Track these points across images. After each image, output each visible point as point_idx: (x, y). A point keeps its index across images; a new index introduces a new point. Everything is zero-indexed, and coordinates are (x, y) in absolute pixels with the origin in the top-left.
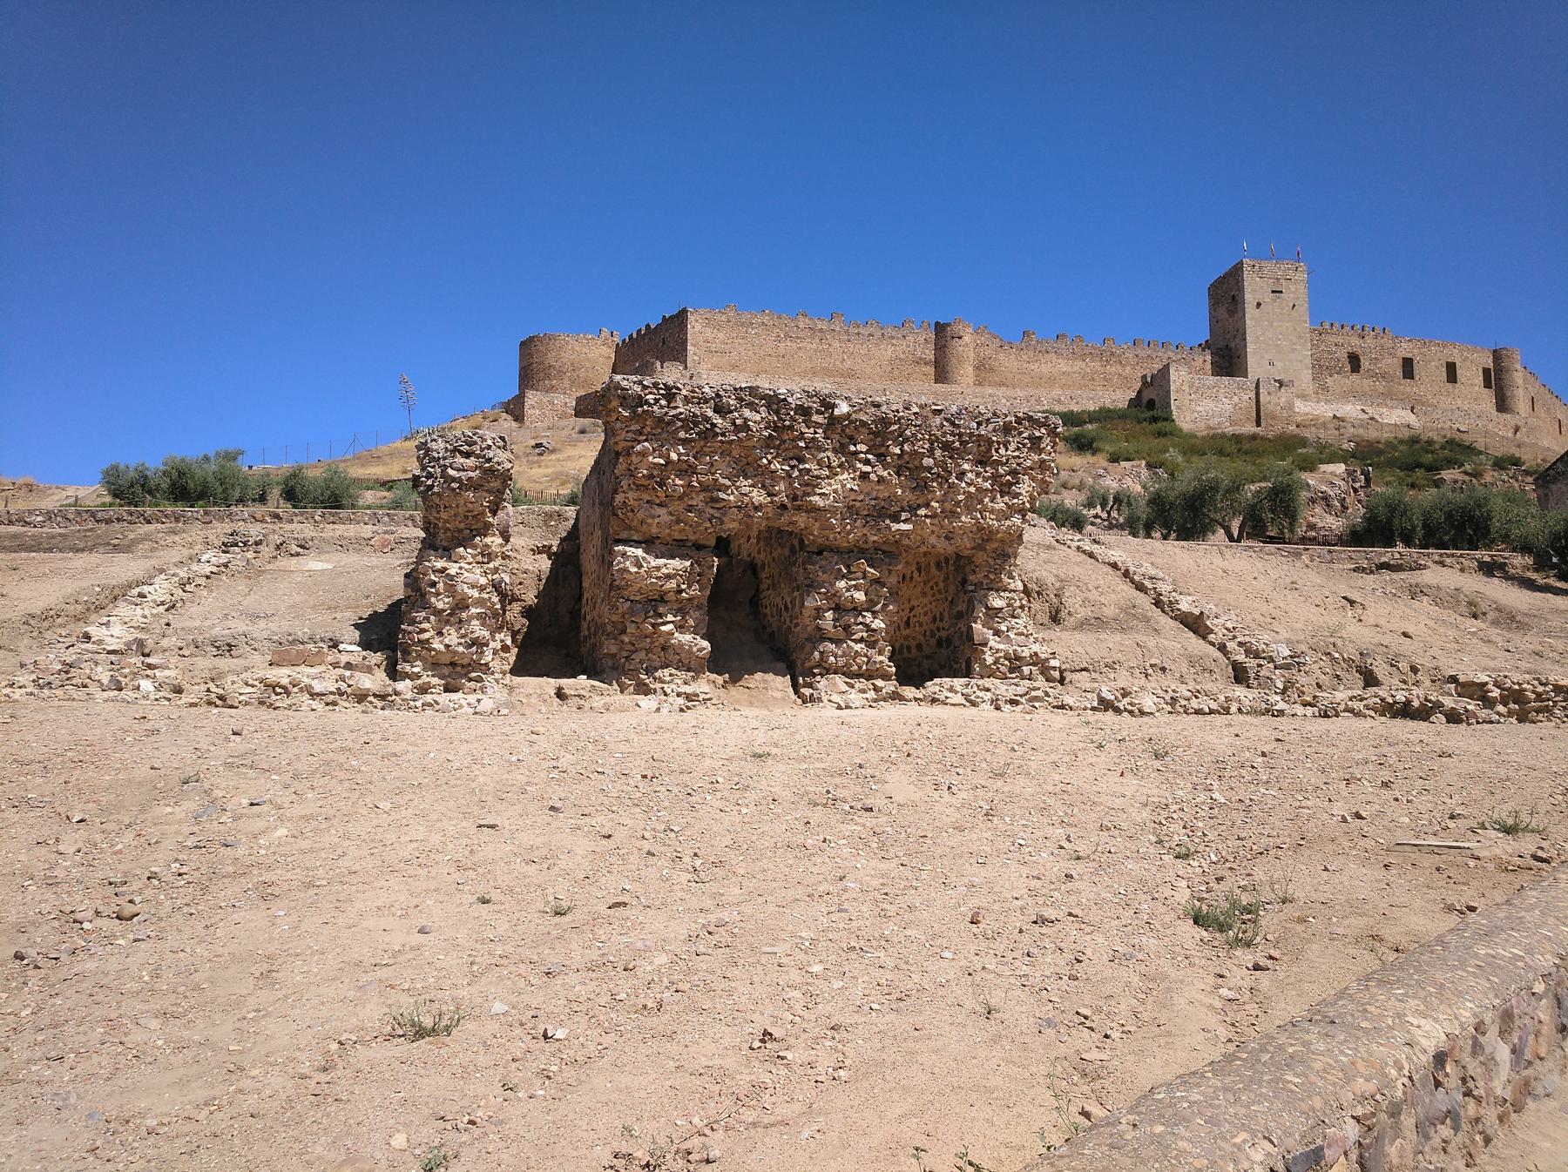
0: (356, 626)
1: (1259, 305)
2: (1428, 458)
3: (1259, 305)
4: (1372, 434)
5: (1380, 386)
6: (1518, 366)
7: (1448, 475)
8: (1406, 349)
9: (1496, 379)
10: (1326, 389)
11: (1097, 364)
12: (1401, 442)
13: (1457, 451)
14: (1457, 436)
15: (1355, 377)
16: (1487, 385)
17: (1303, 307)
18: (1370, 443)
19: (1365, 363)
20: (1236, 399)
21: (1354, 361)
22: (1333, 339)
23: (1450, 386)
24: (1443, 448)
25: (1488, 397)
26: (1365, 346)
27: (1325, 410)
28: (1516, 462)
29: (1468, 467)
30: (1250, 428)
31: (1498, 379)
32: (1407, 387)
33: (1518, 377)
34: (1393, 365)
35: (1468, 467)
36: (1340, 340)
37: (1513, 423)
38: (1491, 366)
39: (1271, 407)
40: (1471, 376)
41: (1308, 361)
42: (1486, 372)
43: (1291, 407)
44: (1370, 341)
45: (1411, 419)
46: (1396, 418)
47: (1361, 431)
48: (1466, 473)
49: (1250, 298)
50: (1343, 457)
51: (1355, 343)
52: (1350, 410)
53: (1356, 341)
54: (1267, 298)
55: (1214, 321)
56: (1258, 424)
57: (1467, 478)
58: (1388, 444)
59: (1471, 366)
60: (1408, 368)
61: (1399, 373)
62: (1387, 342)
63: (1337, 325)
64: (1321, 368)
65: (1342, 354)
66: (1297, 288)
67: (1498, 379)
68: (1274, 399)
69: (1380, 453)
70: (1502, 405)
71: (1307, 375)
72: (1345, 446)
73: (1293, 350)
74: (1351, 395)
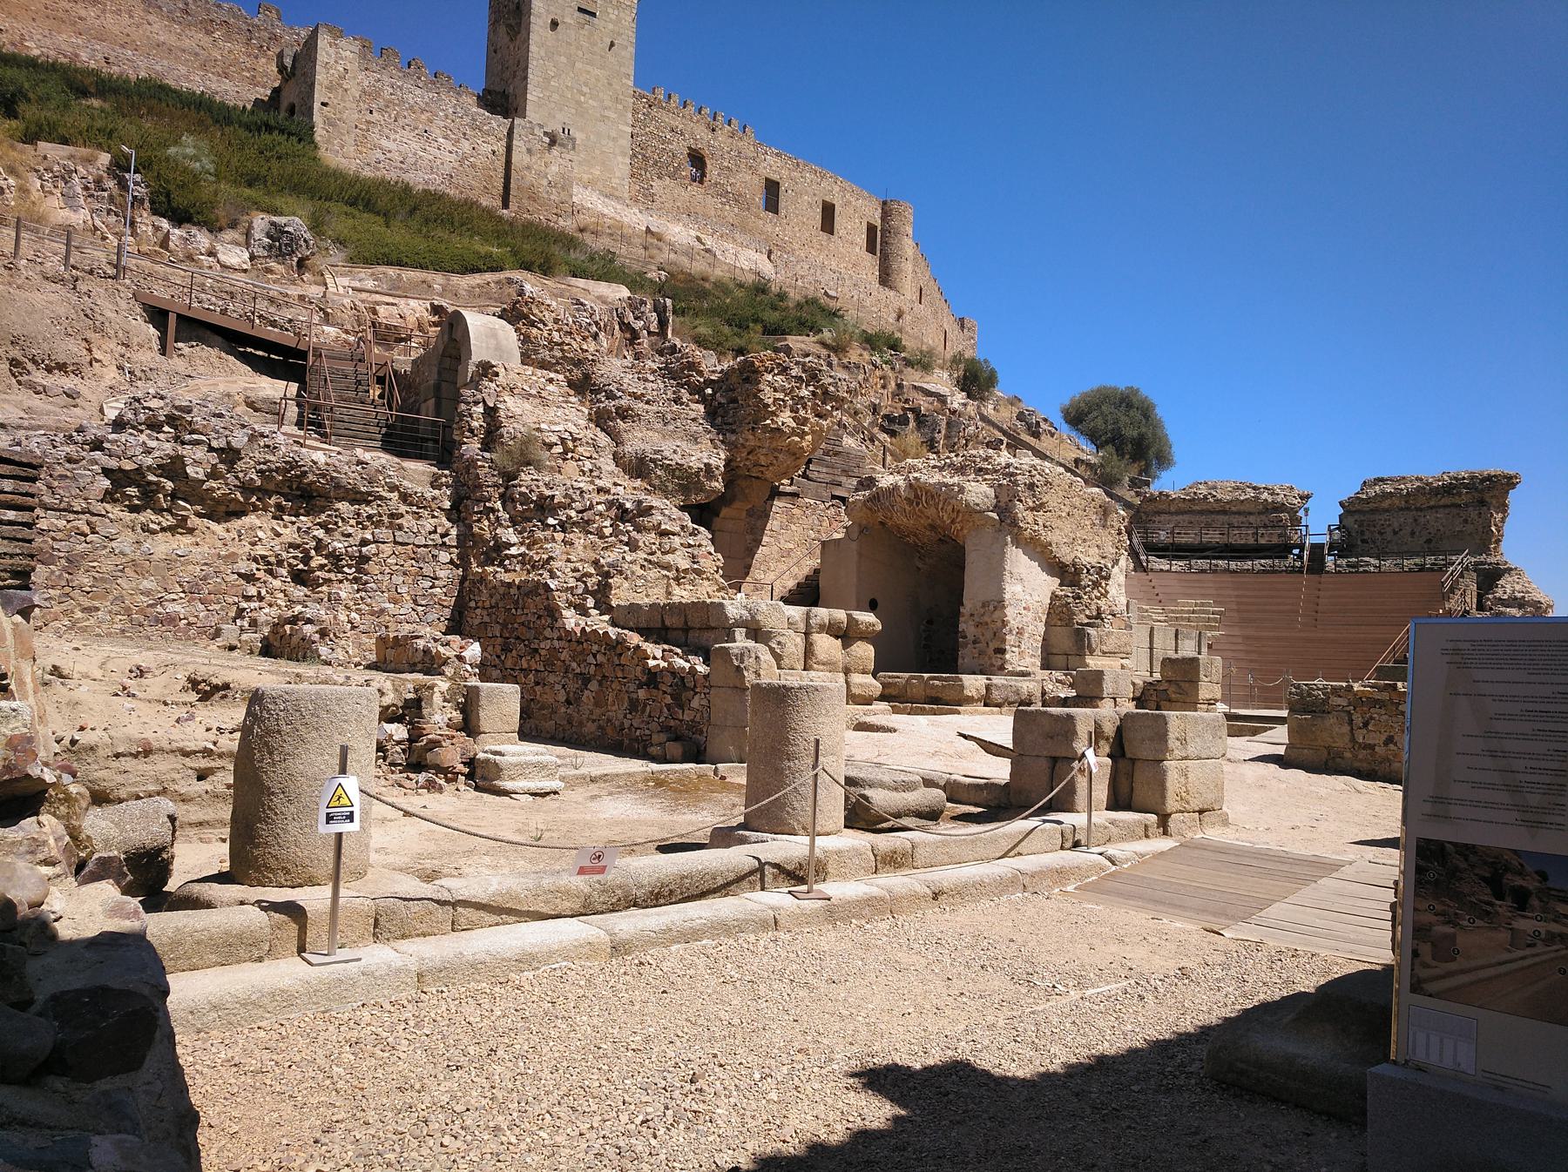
0: (1341, 504)
1: (554, 24)
2: (772, 317)
3: (554, 24)
4: (698, 267)
5: (731, 212)
6: (910, 231)
7: (795, 342)
8: (773, 165)
9: (879, 241)
10: (652, 198)
11: (237, 48)
12: (741, 286)
13: (814, 315)
14: (823, 301)
15: (694, 189)
16: (871, 248)
17: (627, 52)
18: (690, 278)
20: (466, 146)
21: (697, 159)
22: (668, 119)
23: (824, 236)
24: (799, 306)
25: (870, 265)
26: (719, 144)
27: (635, 218)
28: (895, 346)
29: (827, 335)
30: (490, 201)
31: (884, 243)
32: (767, 223)
33: (907, 247)
35: (827, 335)
36: (678, 123)
37: (896, 304)
38: (878, 223)
39: (530, 177)
40: (852, 228)
41: (626, 142)
42: (871, 229)
43: (565, 185)
44: (722, 140)
45: (767, 268)
46: (743, 259)
47: (685, 261)
48: (824, 344)
50: (635, 282)
51: (701, 136)
52: (680, 233)
53: (702, 133)
54: (570, 18)
55: (493, 49)
56: (506, 205)
57: (824, 352)
58: (719, 285)
59: (857, 213)
60: (772, 189)
61: (760, 199)
62: (747, 145)
63: (676, 98)
64: (645, 162)
65: (680, 148)
67: (884, 243)
68: (537, 163)
69: (703, 294)
70: (886, 278)
71: (622, 165)
72: (652, 275)
73: (604, 118)
74: (689, 213)
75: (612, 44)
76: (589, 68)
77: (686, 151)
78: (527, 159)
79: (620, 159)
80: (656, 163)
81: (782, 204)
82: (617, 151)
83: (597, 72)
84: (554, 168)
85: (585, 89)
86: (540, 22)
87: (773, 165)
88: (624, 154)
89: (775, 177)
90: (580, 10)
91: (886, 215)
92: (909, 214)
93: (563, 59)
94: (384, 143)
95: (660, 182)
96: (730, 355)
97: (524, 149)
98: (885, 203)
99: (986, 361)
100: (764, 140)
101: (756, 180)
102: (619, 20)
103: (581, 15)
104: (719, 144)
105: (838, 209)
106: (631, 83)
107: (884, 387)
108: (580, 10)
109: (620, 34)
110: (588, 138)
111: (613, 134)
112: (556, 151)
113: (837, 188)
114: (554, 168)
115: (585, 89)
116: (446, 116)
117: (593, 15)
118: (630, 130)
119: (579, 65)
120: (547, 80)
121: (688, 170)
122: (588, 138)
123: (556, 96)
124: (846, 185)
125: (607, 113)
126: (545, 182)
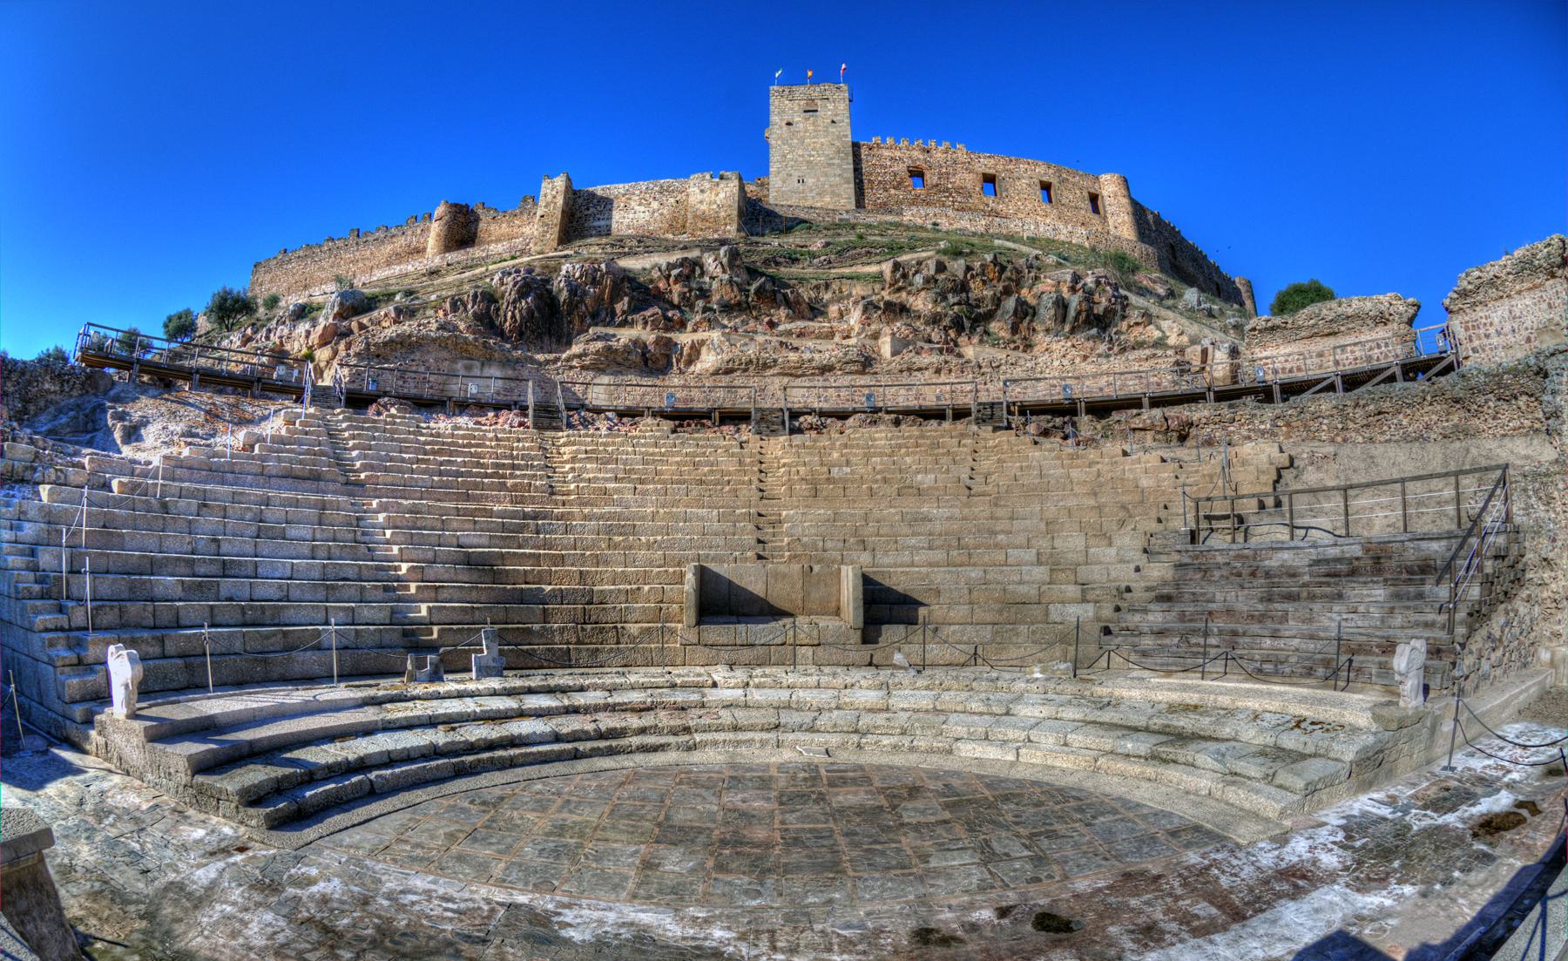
19: (931, 178)
34: (969, 180)
65: (900, 168)
66: (836, 104)
84: (722, 195)
87: (986, 163)
94: (596, 224)
114: (722, 195)
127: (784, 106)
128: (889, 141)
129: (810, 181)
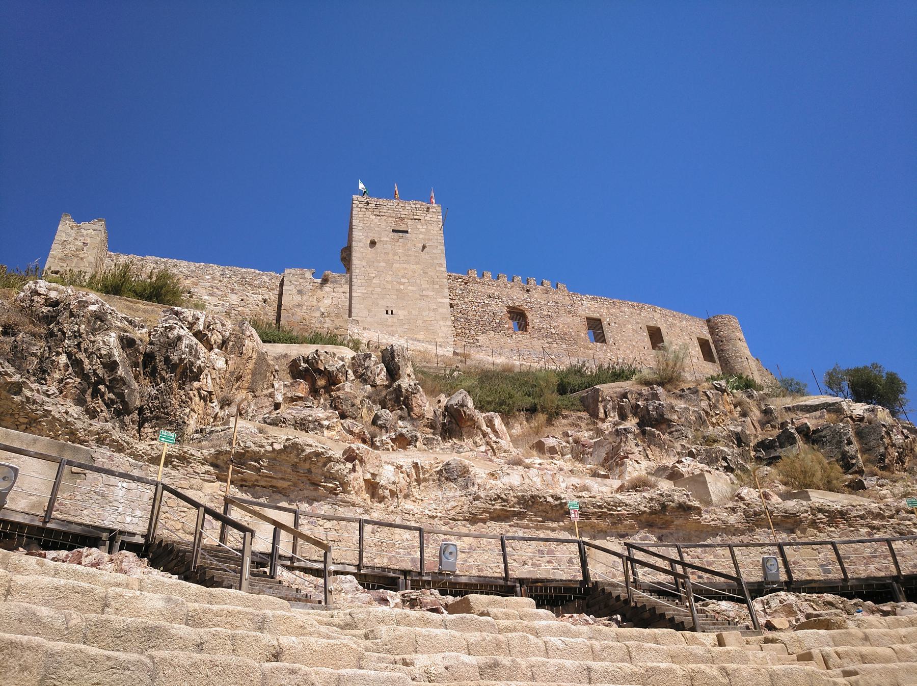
1: (373, 243)
3: (373, 243)
15: (520, 336)
19: (533, 319)
20: (234, 299)
38: (708, 337)
41: (446, 310)
42: (704, 344)
49: (360, 238)
51: (517, 296)
54: (387, 237)
61: (584, 333)
62: (562, 296)
65: (500, 308)
66: (428, 224)
68: (309, 300)
73: (423, 297)
75: (424, 247)
76: (405, 266)
77: (505, 310)
78: (298, 298)
79: (442, 323)
80: (478, 323)
81: (608, 334)
82: (438, 318)
83: (415, 267)
84: (327, 302)
85: (403, 280)
86: (361, 244)
87: (589, 306)
88: (445, 319)
89: (596, 315)
90: (394, 231)
91: (713, 329)
92: (735, 322)
93: (382, 264)
95: (485, 336)
96: (522, 417)
97: (295, 291)
98: (708, 321)
99: (875, 366)
100: (577, 288)
101: (577, 320)
102: (428, 231)
103: (396, 234)
104: (537, 299)
105: (664, 331)
106: (444, 269)
107: (744, 414)
108: (394, 231)
109: (429, 240)
110: (410, 313)
111: (433, 306)
112: (327, 288)
113: (657, 316)
115: (403, 280)
116: (213, 278)
117: (407, 232)
118: (448, 301)
119: (396, 266)
120: (370, 279)
121: (509, 324)
122: (410, 313)
123: (378, 290)
124: (664, 311)
125: (424, 293)
126: (318, 314)
127: (368, 221)
128: (488, 275)
129: (401, 313)
